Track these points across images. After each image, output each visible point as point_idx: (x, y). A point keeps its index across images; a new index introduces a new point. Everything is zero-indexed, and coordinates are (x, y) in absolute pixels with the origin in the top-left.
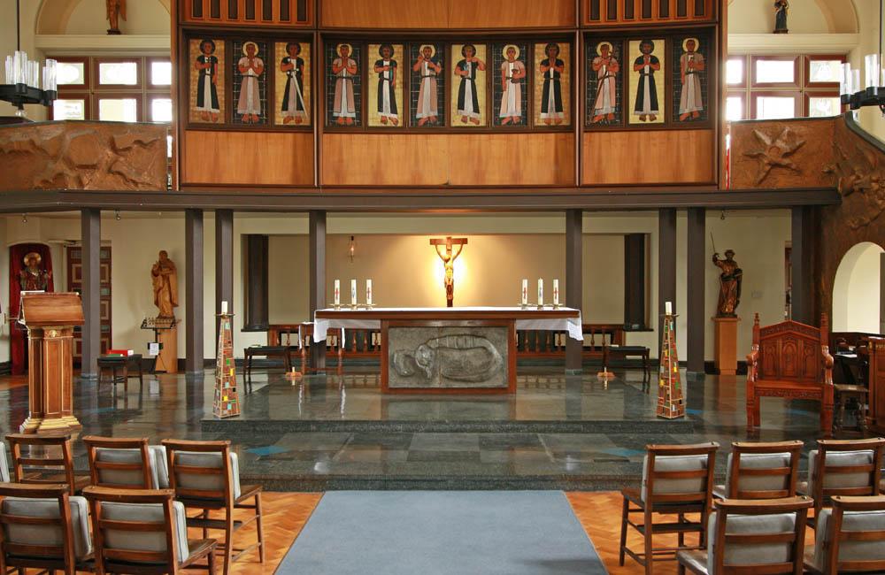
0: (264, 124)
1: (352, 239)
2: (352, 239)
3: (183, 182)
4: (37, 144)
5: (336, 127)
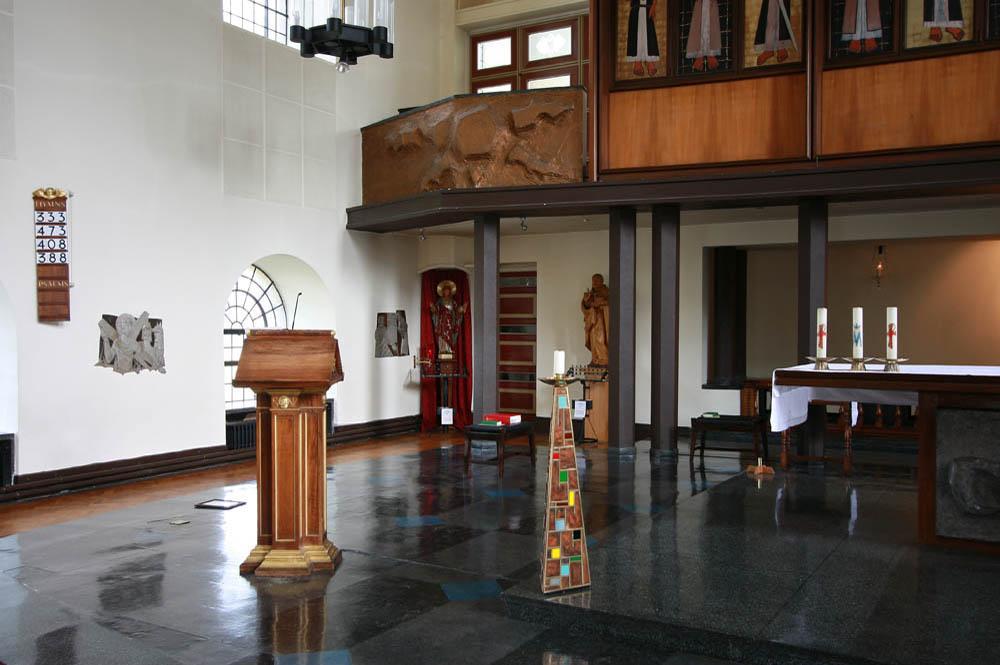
0: (727, 68)
1: (880, 252)
2: (880, 252)
3: (604, 167)
4: (425, 133)
5: (844, 57)
